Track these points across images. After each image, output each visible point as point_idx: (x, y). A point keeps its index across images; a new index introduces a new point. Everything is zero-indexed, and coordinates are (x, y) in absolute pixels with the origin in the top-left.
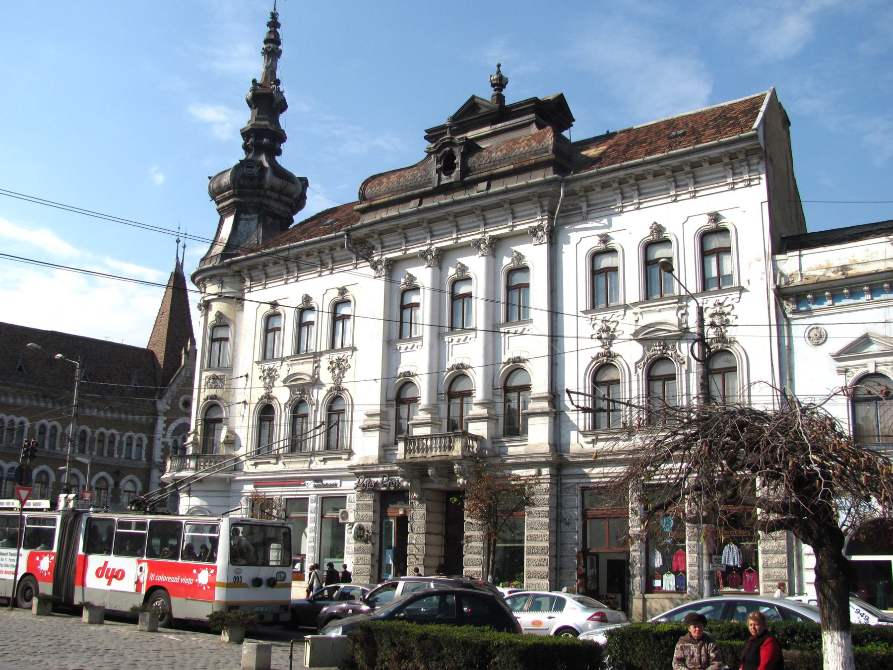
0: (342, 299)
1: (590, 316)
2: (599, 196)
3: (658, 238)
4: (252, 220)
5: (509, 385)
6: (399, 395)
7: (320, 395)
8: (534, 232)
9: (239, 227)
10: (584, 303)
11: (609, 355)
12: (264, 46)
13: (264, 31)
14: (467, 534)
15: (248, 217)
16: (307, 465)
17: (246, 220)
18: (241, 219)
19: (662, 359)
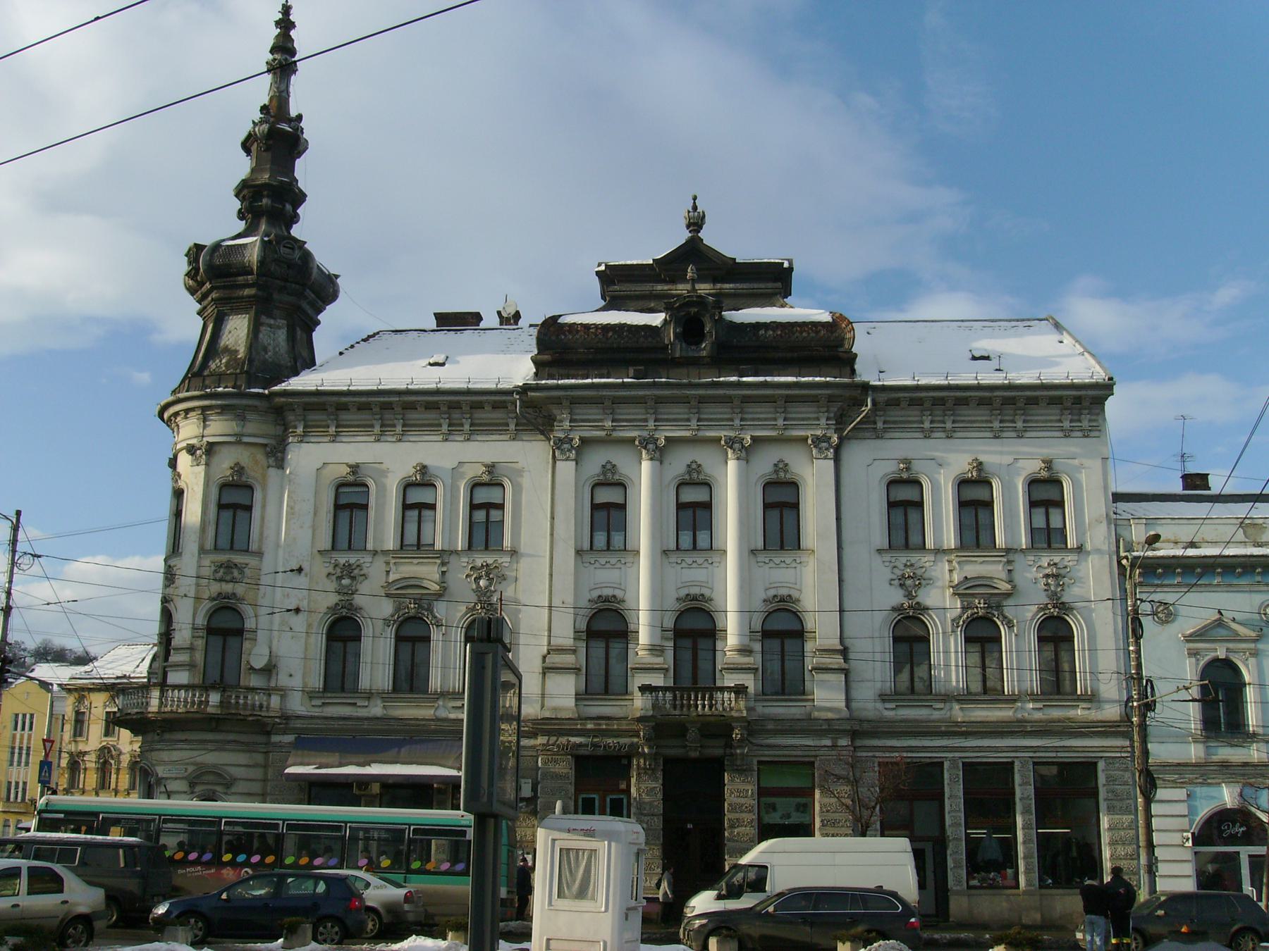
0: (492, 479)
1: (887, 557)
2: (903, 412)
3: (423, 479)
4: (279, 328)
5: (780, 628)
6: (605, 625)
7: (453, 617)
8: (817, 441)
9: (261, 336)
10: (879, 537)
11: (351, 607)
12: (270, 57)
13: (271, 33)
14: (728, 816)
15: (272, 322)
16: (432, 712)
17: (270, 326)
18: (262, 324)
19: (417, 619)
